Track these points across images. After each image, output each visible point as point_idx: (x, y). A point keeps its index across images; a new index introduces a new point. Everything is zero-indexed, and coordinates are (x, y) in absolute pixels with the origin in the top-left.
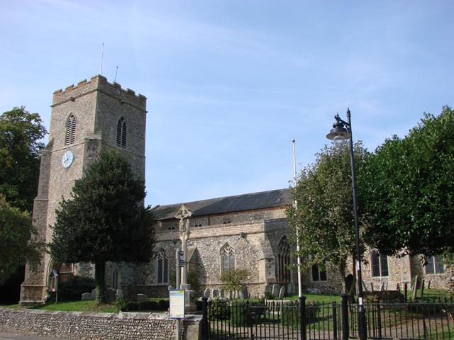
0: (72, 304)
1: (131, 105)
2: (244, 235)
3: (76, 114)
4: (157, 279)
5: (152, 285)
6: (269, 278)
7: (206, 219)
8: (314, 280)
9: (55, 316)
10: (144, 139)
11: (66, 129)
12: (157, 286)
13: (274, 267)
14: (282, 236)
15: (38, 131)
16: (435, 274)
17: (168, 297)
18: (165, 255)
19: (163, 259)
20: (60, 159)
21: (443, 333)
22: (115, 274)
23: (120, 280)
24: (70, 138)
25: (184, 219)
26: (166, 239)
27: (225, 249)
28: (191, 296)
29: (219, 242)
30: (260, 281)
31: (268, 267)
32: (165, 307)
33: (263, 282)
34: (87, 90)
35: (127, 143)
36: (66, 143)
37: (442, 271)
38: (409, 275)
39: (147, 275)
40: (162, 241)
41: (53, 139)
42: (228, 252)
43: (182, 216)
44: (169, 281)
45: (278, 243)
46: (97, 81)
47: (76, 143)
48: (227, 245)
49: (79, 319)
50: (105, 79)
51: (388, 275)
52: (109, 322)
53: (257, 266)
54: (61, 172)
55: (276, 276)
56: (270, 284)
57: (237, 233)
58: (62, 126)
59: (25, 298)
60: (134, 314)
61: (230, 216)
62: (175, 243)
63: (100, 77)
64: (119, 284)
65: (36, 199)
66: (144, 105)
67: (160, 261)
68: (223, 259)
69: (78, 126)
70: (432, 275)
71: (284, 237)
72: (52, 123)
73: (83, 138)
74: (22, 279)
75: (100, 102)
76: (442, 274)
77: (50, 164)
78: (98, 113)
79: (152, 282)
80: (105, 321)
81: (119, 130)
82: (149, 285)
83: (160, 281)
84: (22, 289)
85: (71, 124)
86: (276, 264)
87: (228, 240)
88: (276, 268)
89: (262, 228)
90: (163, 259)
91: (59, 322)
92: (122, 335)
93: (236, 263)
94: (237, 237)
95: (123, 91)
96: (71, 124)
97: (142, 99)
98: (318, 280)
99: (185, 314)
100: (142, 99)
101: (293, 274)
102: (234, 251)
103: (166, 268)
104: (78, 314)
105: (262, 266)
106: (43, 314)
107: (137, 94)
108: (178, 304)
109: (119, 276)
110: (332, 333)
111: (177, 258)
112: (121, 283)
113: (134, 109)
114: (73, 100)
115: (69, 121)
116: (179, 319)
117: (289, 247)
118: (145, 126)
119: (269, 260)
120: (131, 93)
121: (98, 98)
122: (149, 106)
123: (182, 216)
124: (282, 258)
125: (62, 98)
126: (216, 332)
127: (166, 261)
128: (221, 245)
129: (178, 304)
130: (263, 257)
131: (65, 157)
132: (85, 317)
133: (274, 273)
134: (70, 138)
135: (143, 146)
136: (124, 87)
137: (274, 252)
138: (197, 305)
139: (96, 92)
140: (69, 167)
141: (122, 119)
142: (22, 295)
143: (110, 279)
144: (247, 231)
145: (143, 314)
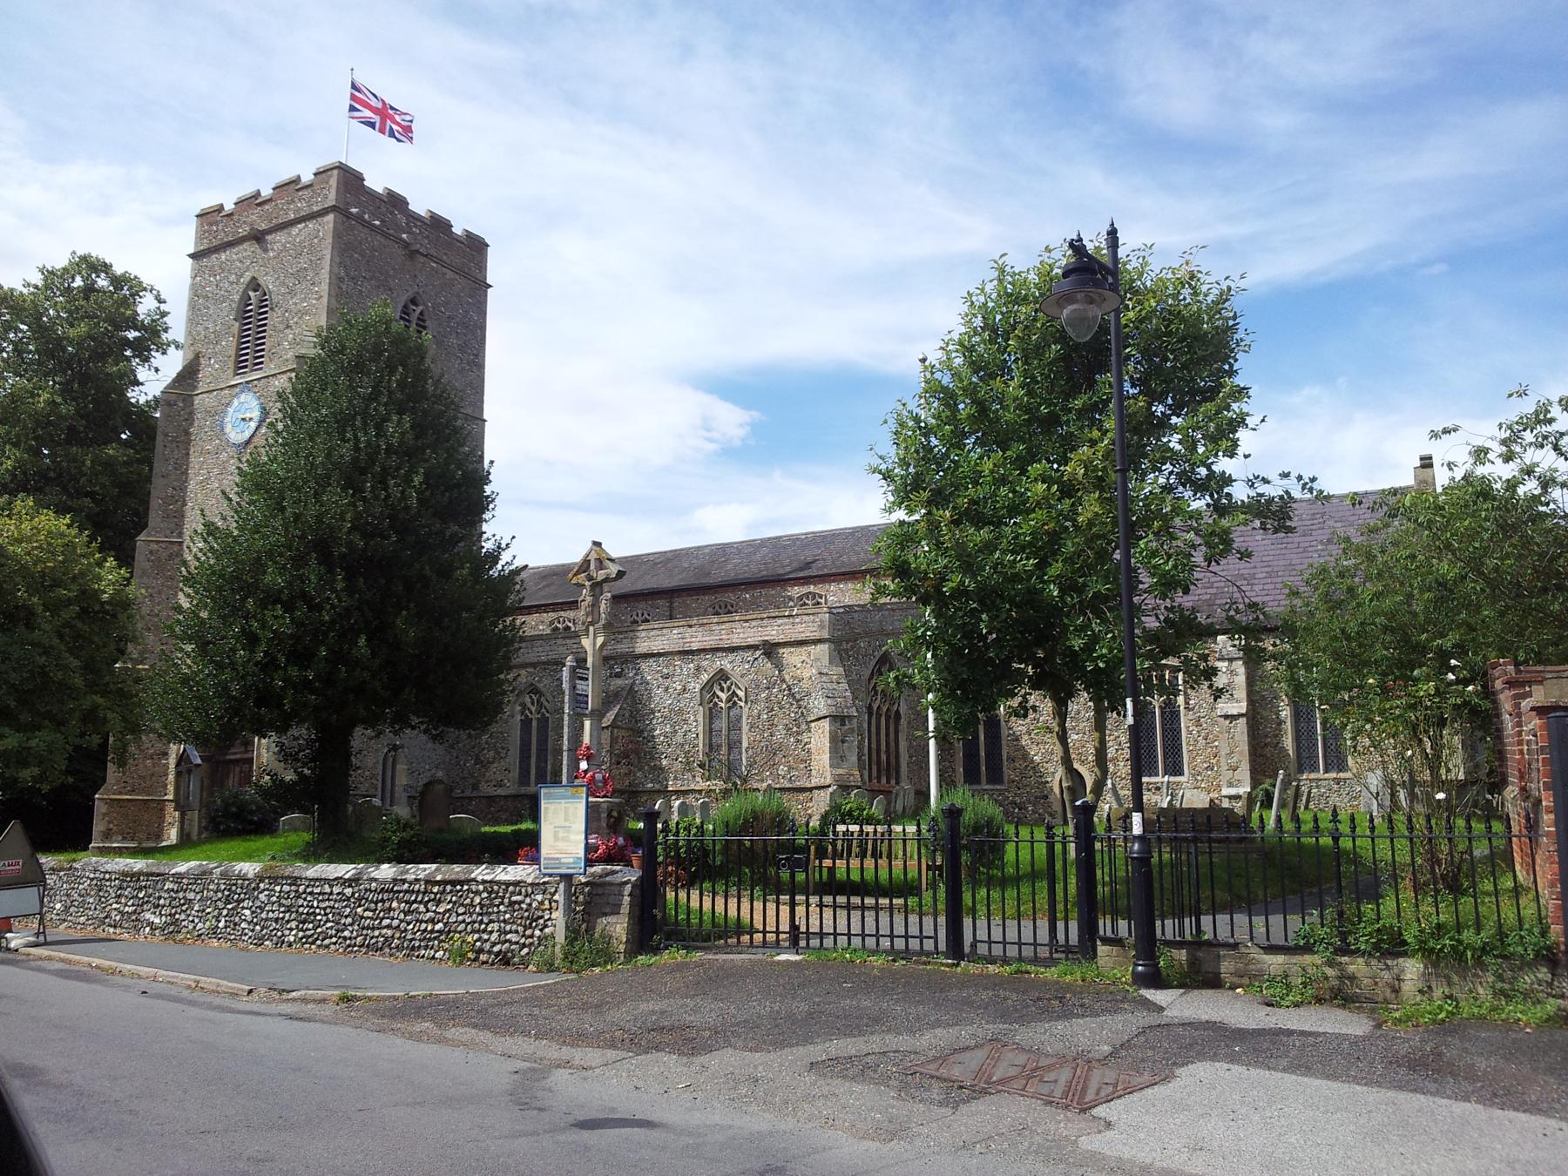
0: (238, 845)
1: (439, 261)
2: (770, 650)
3: (268, 282)
4: (515, 774)
5: (500, 792)
6: (840, 771)
7: (662, 603)
9: (178, 877)
11: (237, 324)
12: (515, 797)
13: (854, 740)
14: (878, 654)
15: (151, 338)
16: (1321, 775)
17: (535, 817)
18: (540, 705)
20: (218, 413)
21: (1493, 875)
22: (389, 765)
23: (402, 780)
24: (248, 354)
25: (593, 587)
28: (609, 816)
29: (698, 669)
30: (814, 782)
31: (837, 742)
32: (524, 846)
33: (822, 782)
34: (303, 207)
36: (240, 366)
37: (1342, 767)
38: (1244, 773)
39: (485, 765)
40: (534, 665)
41: (197, 357)
42: (723, 696)
43: (590, 578)
44: (541, 767)
45: (867, 673)
46: (333, 182)
47: (270, 368)
48: (722, 676)
49: (250, 887)
50: (359, 178)
51: (1181, 774)
52: (348, 891)
54: (224, 456)
55: (861, 769)
56: (844, 788)
57: (751, 641)
58: (224, 316)
59: (107, 835)
60: (426, 870)
61: (730, 597)
63: (342, 168)
65: (142, 537)
66: (482, 265)
67: (526, 723)
68: (712, 715)
69: (274, 319)
70: (1312, 776)
72: (193, 306)
73: (290, 354)
75: (344, 246)
76: (1342, 775)
77: (187, 433)
78: (337, 282)
79: (500, 784)
80: (336, 890)
82: (492, 791)
84: (100, 808)
85: (253, 315)
87: (725, 662)
88: (860, 747)
89: (822, 627)
91: (191, 896)
92: (390, 932)
93: (745, 728)
94: (748, 655)
96: (253, 315)
97: (475, 247)
99: (589, 862)
100: (475, 247)
102: (741, 694)
104: (250, 868)
105: (820, 738)
106: (140, 873)
108: (564, 827)
109: (401, 767)
110: (1043, 925)
111: (565, 686)
113: (450, 275)
114: (258, 237)
115: (246, 300)
116: (567, 878)
118: (483, 328)
119: (838, 719)
120: (438, 224)
121: (337, 235)
122: (496, 270)
123: (590, 578)
124: (879, 716)
125: (224, 233)
126: (695, 921)
128: (705, 677)
129: (564, 827)
130: (824, 712)
131: (232, 415)
132: (275, 880)
133: (855, 758)
134: (248, 354)
136: (419, 206)
137: (855, 698)
138: (623, 825)
139: (330, 217)
140: (248, 442)
141: (414, 301)
142: (98, 827)
143: (373, 776)
144: (781, 638)
145: (457, 870)
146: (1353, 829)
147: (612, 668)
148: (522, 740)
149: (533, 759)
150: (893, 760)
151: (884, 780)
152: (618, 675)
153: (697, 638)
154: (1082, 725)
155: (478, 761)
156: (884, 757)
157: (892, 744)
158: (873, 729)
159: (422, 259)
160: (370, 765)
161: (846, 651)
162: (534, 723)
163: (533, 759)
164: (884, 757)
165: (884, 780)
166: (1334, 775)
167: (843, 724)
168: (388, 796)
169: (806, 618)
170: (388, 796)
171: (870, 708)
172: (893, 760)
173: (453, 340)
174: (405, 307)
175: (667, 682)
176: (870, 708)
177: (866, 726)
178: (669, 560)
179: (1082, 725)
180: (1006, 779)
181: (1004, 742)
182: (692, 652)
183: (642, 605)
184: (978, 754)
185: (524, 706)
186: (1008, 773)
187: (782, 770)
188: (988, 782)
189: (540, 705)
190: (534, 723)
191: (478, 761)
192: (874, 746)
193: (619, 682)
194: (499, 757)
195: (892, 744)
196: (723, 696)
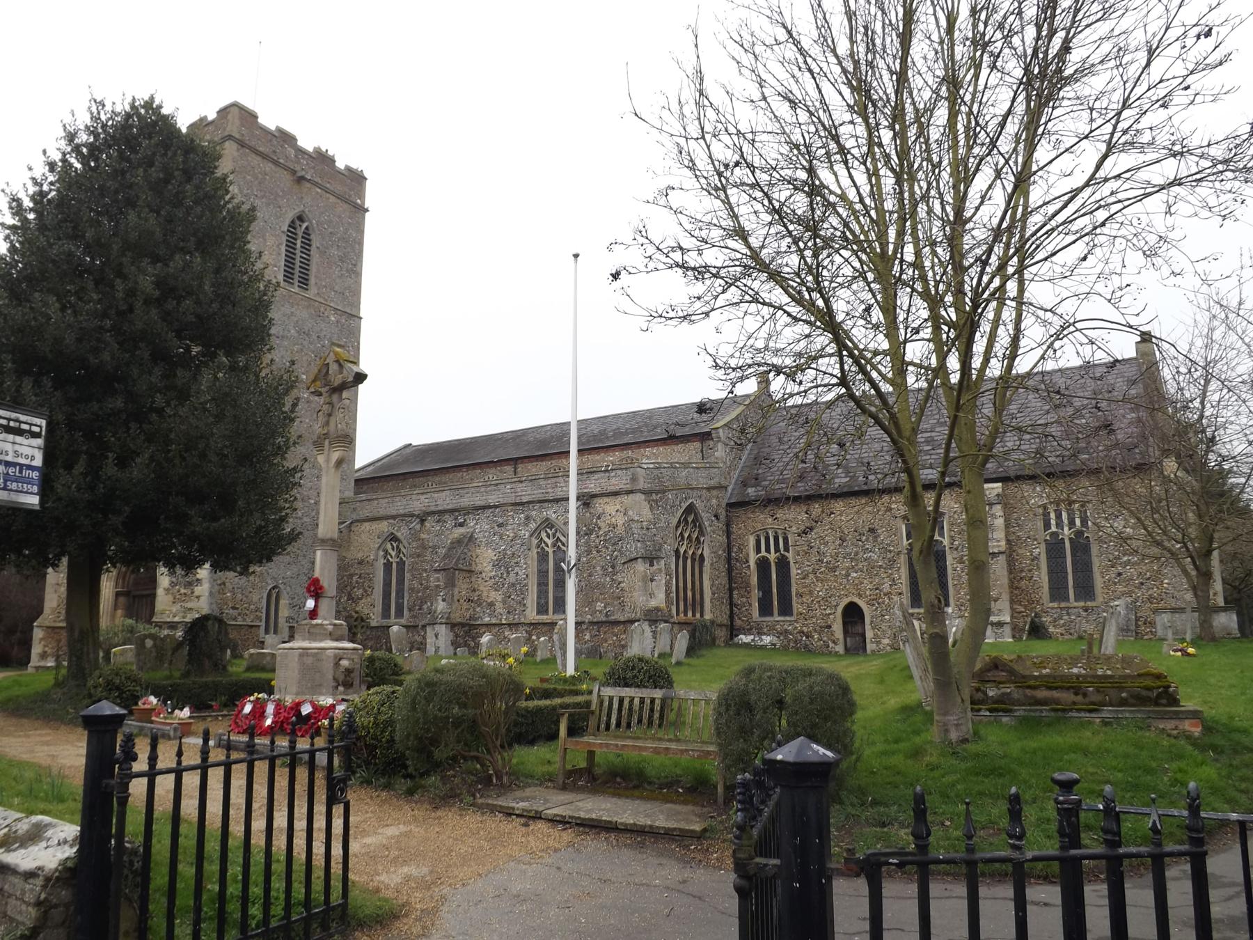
4: (379, 608)
8: (1053, 598)
10: (358, 275)
13: (661, 579)
14: (684, 506)
18: (399, 551)
19: (394, 560)
26: (402, 512)
27: (543, 535)
29: (527, 518)
35: (312, 281)
50: (254, 116)
53: (619, 577)
62: (423, 521)
64: (282, 621)
66: (361, 193)
71: (690, 509)
74: (39, 611)
81: (291, 246)
83: (542, 609)
84: (38, 634)
86: (668, 574)
88: (668, 585)
90: (394, 560)
95: (302, 151)
97: (356, 179)
98: (771, 614)
100: (356, 179)
101: (555, 598)
103: (401, 581)
107: (340, 164)
112: (289, 619)
113: (332, 199)
117: (701, 533)
118: (361, 243)
120: (323, 159)
122: (371, 198)
124: (685, 559)
127: (401, 564)
128: (533, 526)
135: (356, 293)
141: (301, 218)
144: (597, 490)
146: (1114, 839)
147: (456, 519)
148: (384, 580)
149: (393, 595)
150: (698, 597)
151: (690, 614)
152: (461, 525)
153: (527, 493)
154: (860, 565)
155: (350, 598)
156: (690, 594)
157: (697, 583)
158: (681, 570)
159: (308, 185)
160: (255, 598)
161: (656, 501)
162: (394, 566)
163: (393, 595)
164: (690, 594)
165: (690, 614)
166: (1082, 604)
167: (651, 565)
168: (272, 625)
169: (619, 472)
170: (272, 625)
171: (677, 551)
172: (698, 597)
173: (334, 251)
174: (293, 222)
175: (502, 530)
176: (677, 551)
177: (673, 567)
178: (518, 437)
179: (860, 565)
180: (795, 612)
181: (793, 581)
182: (522, 504)
183: (493, 470)
184: (771, 591)
185: (386, 552)
186: (797, 606)
187: (599, 606)
188: (780, 615)
189: (399, 551)
190: (394, 566)
191: (350, 598)
192: (681, 585)
193: (462, 530)
194: (366, 594)
195: (697, 583)
196: (549, 542)
